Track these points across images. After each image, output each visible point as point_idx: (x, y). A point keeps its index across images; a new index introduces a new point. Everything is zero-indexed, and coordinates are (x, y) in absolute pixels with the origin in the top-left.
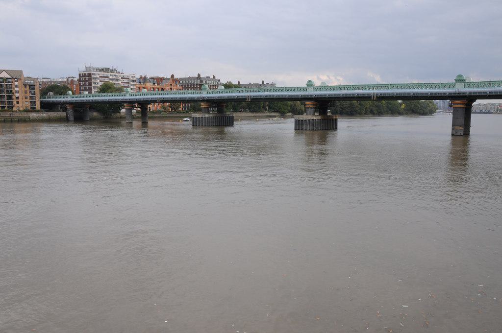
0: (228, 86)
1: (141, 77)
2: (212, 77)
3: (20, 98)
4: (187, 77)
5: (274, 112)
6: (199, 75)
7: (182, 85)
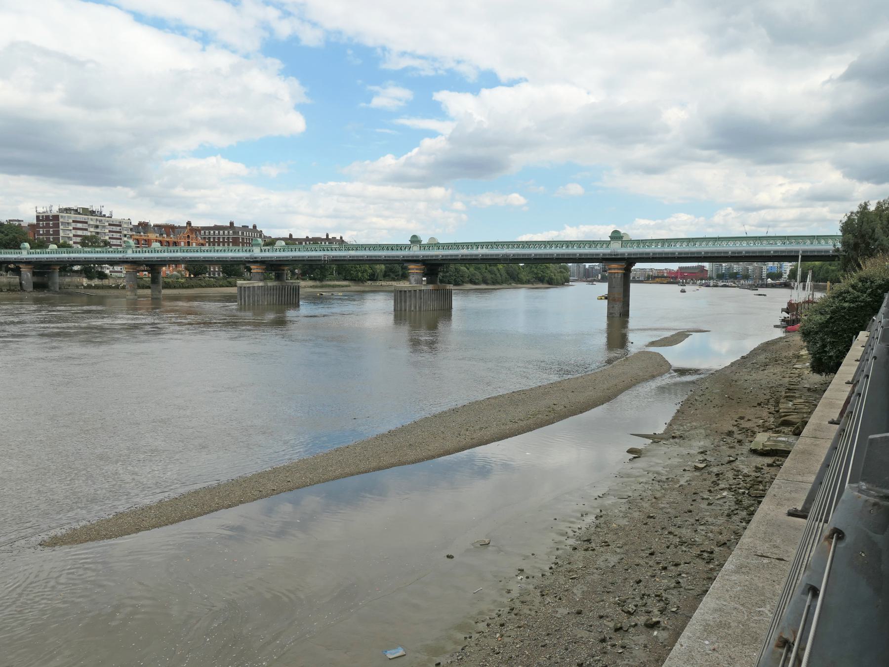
0: (290, 241)
2: (251, 227)
5: (345, 279)
7: (205, 238)
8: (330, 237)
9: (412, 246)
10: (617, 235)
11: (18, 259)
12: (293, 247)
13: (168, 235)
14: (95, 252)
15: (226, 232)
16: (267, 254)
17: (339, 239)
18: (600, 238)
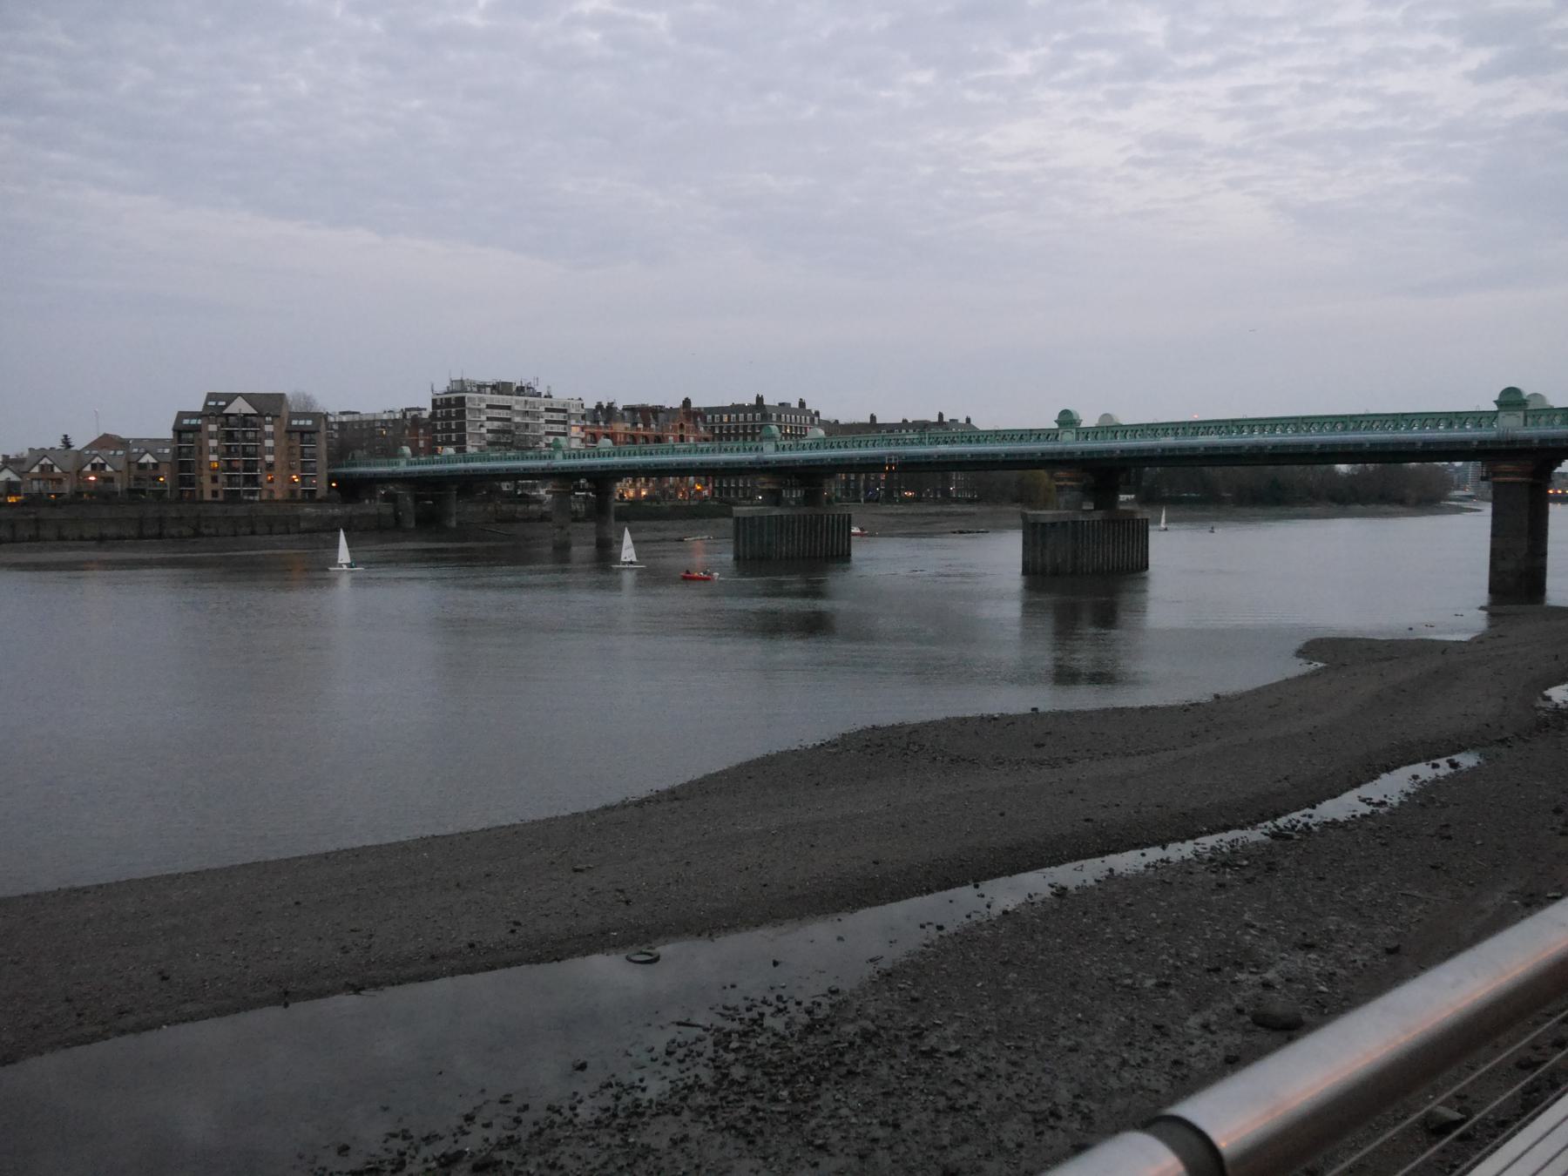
1: (599, 406)
2: (795, 405)
3: (278, 466)
4: (729, 404)
6: (760, 399)
8: (945, 420)
9: (1060, 431)
11: (549, 469)
12: (834, 441)
13: (646, 425)
14: (696, 451)
15: (741, 415)
16: (787, 455)
17: (965, 422)
18: (240, 410)
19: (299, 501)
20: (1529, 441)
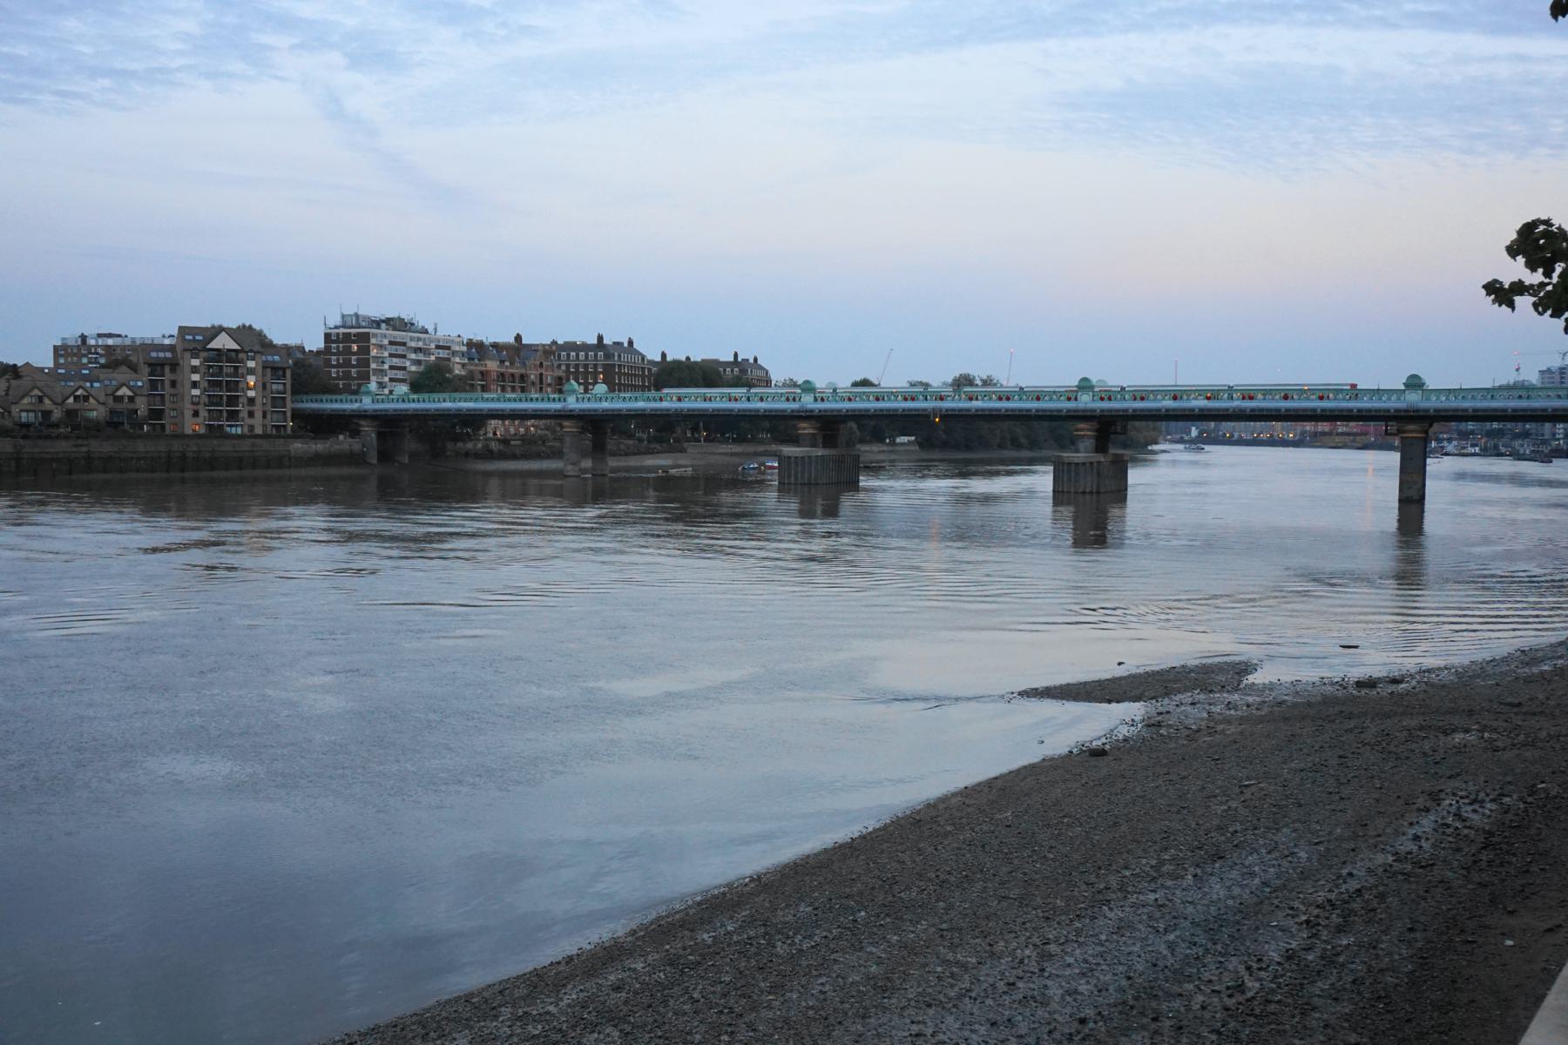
3: (259, 401)
10: (1416, 381)
11: (565, 411)
19: (288, 437)
20: (1427, 410)
